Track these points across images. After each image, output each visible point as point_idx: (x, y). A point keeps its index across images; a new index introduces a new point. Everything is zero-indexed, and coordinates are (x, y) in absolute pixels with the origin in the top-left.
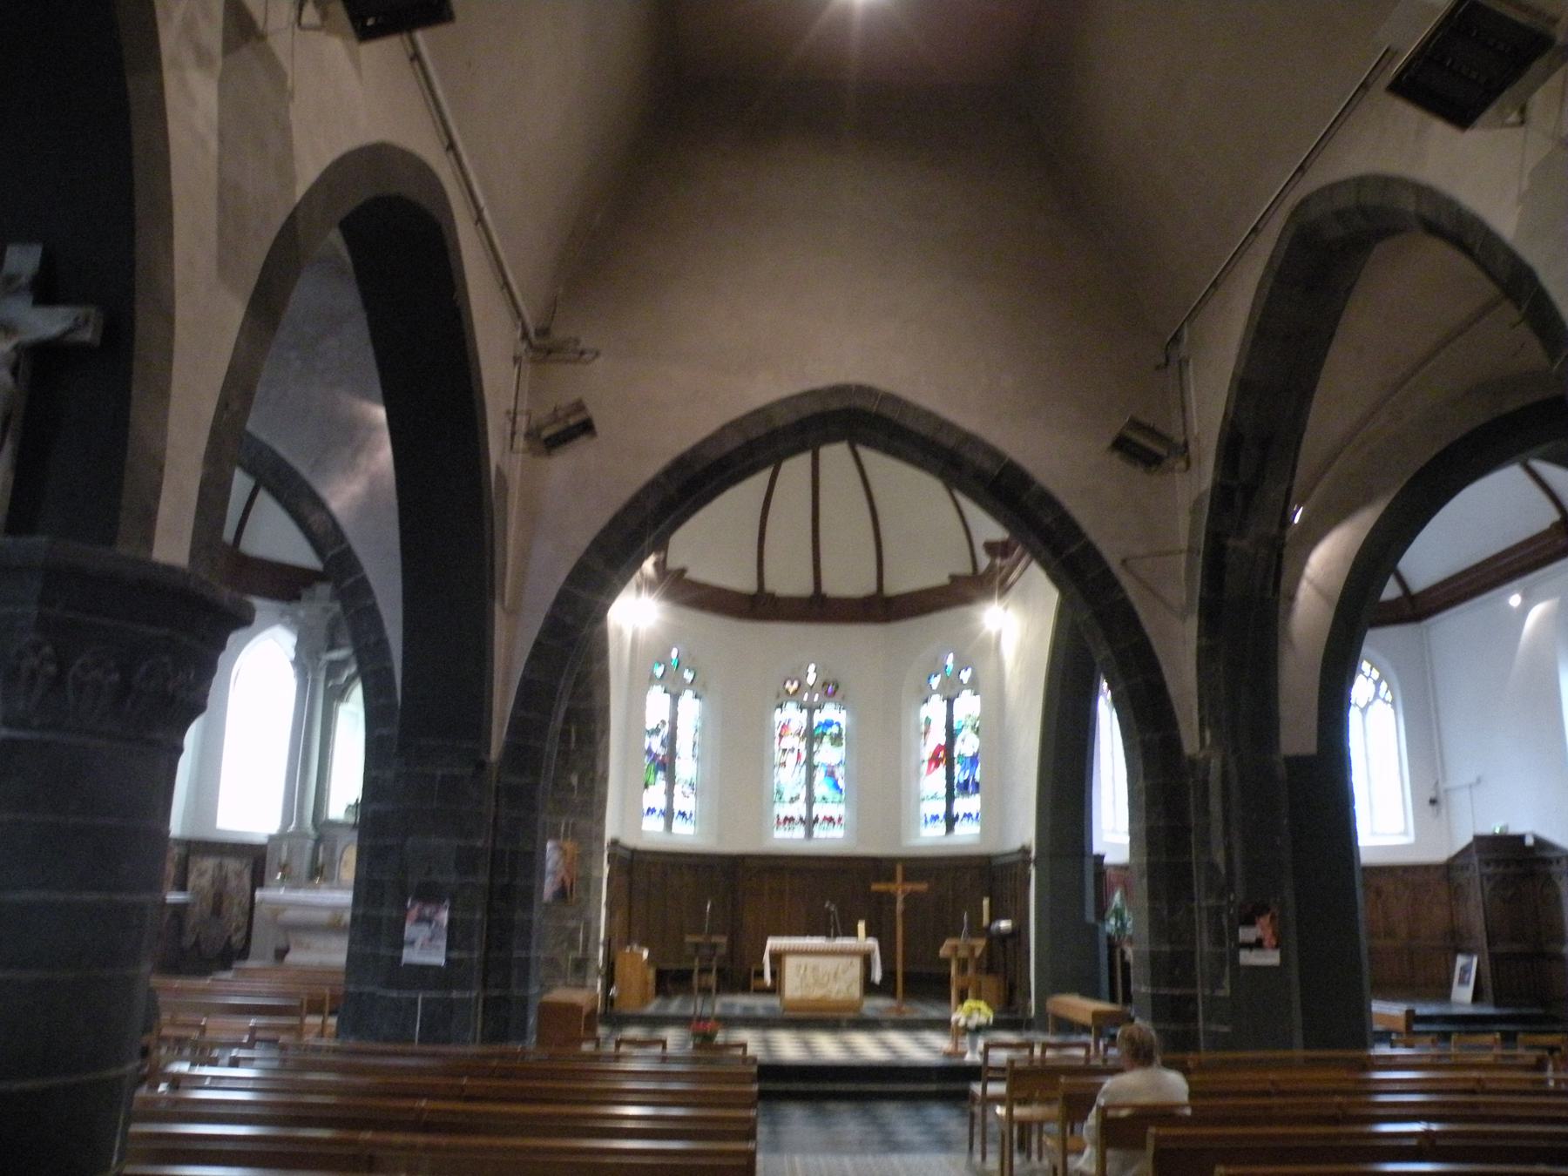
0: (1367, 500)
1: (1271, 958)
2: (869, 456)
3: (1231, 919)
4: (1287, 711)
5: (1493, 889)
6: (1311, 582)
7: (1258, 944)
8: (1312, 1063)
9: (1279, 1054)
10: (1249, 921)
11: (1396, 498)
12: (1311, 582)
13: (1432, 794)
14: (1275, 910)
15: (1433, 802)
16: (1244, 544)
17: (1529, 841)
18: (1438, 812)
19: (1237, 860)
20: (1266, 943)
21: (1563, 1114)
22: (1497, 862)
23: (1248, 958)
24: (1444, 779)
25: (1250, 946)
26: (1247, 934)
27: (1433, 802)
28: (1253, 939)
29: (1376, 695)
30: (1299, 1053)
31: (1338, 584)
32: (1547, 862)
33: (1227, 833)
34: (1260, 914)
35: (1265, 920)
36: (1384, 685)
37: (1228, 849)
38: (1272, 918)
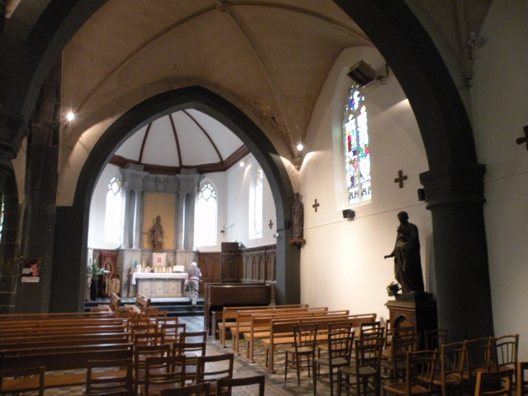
0: (111, 115)
1: (35, 280)
2: (188, 111)
3: (20, 265)
4: (60, 189)
5: (225, 260)
6: (81, 143)
7: (31, 275)
8: (50, 317)
9: (74, 313)
10: (28, 266)
11: (122, 116)
12: (81, 143)
13: (223, 230)
14: (39, 262)
15: (222, 232)
16: (39, 125)
17: (240, 245)
18: (224, 236)
19: (26, 243)
20: (34, 274)
21: (2, 339)
22: (228, 252)
23: (25, 280)
24: (227, 224)
25: (27, 275)
26: (26, 271)
27: (222, 232)
28: (28, 273)
29: (211, 196)
30: (45, 314)
31: (92, 145)
32: (241, 251)
33: (23, 233)
34: (33, 264)
35: (35, 266)
36: (214, 192)
37: (23, 240)
38: (38, 265)
